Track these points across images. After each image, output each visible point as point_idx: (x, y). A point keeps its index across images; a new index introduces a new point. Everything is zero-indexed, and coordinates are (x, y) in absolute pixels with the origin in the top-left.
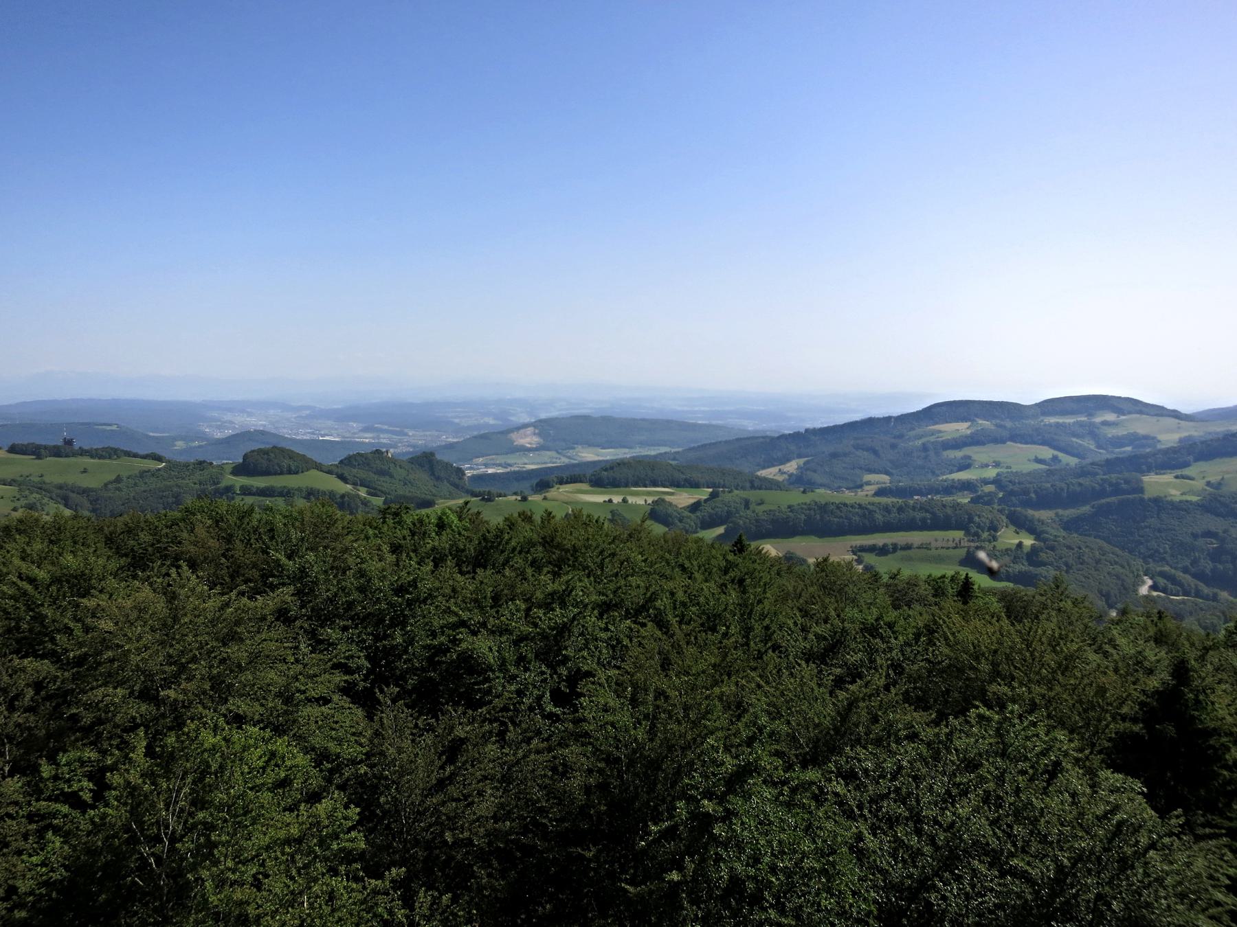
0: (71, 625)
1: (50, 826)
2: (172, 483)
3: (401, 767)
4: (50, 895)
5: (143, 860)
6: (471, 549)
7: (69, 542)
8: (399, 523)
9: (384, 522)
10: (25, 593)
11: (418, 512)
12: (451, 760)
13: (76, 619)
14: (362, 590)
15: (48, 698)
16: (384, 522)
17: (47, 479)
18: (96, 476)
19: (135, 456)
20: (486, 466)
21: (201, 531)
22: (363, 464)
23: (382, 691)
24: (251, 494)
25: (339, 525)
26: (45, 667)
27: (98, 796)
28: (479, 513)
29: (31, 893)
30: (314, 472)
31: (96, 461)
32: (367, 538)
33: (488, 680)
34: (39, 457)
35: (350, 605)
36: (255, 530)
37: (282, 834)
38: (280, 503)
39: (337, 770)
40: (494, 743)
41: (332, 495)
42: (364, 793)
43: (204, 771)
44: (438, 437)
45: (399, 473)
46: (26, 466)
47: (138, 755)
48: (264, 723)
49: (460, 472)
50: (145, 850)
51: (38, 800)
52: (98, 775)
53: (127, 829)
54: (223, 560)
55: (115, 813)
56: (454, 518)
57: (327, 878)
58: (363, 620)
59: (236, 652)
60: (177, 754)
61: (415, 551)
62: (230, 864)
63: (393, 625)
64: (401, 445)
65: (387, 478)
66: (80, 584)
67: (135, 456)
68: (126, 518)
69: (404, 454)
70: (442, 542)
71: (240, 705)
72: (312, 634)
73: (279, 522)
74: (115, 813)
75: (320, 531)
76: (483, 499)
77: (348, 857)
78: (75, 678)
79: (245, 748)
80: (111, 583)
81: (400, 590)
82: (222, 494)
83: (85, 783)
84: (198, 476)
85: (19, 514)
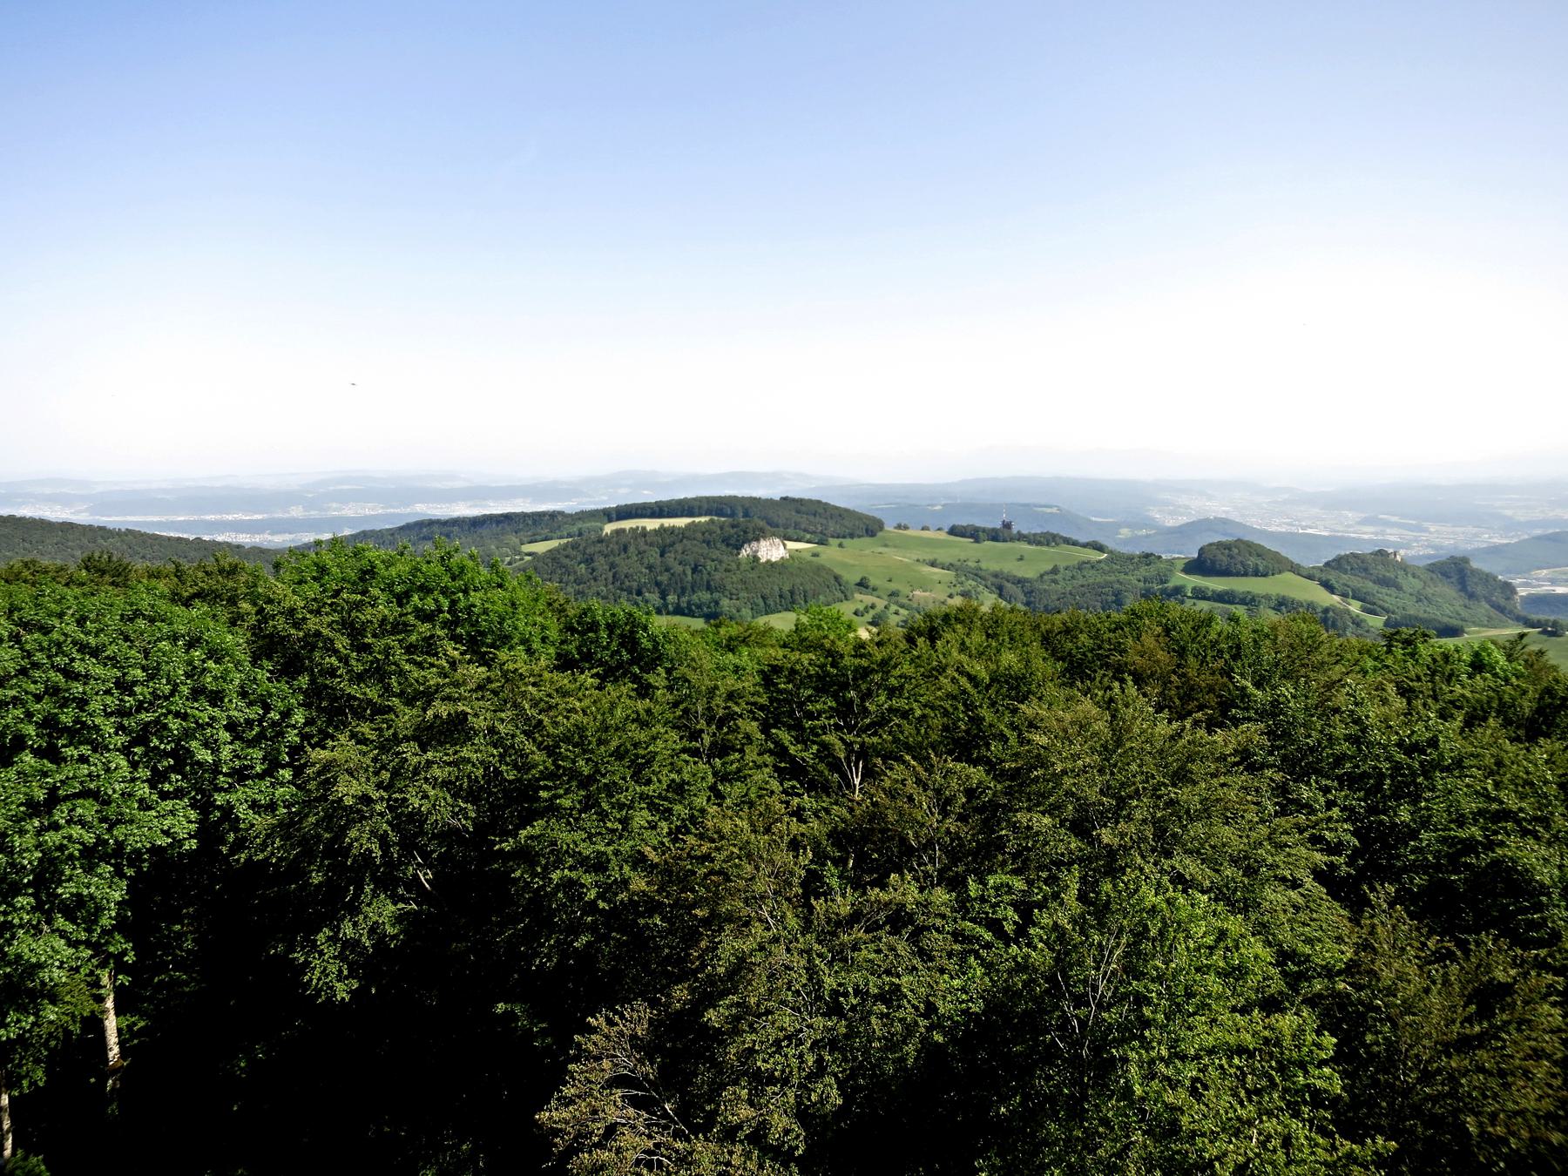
0: (1007, 732)
1: (976, 953)
2: (1113, 578)
3: (1404, 1002)
4: (967, 1026)
5: (1066, 1020)
6: (1527, 706)
7: (1007, 638)
8: (1412, 655)
9: (1389, 652)
10: (964, 692)
11: (1443, 641)
12: (1485, 1013)
13: (1013, 727)
14: (1353, 740)
15: (978, 810)
16: (1389, 652)
17: (984, 565)
18: (1030, 565)
19: (1075, 543)
20: (1553, 582)
21: (1149, 641)
22: (1360, 570)
23: (1373, 889)
24: (1205, 598)
25: (1324, 649)
26: (977, 774)
27: (1021, 931)
28: (1541, 653)
29: (950, 1018)
30: (1288, 576)
31: (1033, 547)
32: (1365, 673)
33: (1539, 907)
34: (977, 540)
35: (1339, 760)
36: (1214, 644)
37: (1231, 1040)
38: (1240, 611)
39: (1301, 976)
40: (1554, 1004)
41: (1311, 606)
42: (1343, 1018)
43: (1141, 934)
44: (1476, 535)
45: (1410, 584)
46: (966, 549)
47: (1071, 896)
48: (1221, 894)
49: (1508, 589)
50: (1070, 1010)
51: (963, 919)
52: (1025, 909)
53: (1051, 979)
54: (1174, 678)
55: (1041, 957)
56: (1499, 658)
57: (1285, 1117)
58: (1352, 781)
59: (1186, 795)
60: (1114, 907)
61: (1435, 698)
62: (1164, 1053)
63: (1397, 795)
64: (1417, 545)
65: (1393, 591)
66: (1016, 687)
67: (1075, 543)
68: (1064, 616)
69: (1420, 558)
70: (1466, 688)
71: (1191, 867)
72: (1282, 790)
73: (1246, 637)
74: (1041, 957)
75: (1299, 659)
76: (1545, 632)
77: (1318, 1098)
78: (1008, 792)
79: (1192, 918)
80: (1051, 690)
81: (1412, 749)
82: (1169, 596)
83: (1010, 912)
84: (1143, 571)
85: (958, 601)
